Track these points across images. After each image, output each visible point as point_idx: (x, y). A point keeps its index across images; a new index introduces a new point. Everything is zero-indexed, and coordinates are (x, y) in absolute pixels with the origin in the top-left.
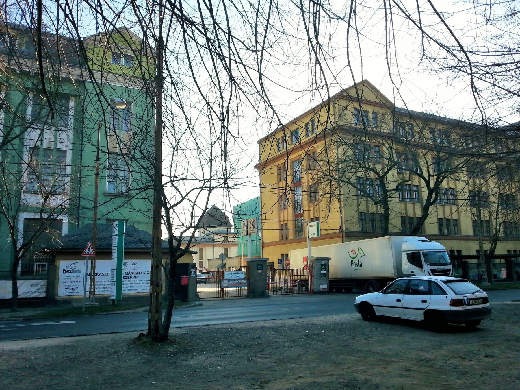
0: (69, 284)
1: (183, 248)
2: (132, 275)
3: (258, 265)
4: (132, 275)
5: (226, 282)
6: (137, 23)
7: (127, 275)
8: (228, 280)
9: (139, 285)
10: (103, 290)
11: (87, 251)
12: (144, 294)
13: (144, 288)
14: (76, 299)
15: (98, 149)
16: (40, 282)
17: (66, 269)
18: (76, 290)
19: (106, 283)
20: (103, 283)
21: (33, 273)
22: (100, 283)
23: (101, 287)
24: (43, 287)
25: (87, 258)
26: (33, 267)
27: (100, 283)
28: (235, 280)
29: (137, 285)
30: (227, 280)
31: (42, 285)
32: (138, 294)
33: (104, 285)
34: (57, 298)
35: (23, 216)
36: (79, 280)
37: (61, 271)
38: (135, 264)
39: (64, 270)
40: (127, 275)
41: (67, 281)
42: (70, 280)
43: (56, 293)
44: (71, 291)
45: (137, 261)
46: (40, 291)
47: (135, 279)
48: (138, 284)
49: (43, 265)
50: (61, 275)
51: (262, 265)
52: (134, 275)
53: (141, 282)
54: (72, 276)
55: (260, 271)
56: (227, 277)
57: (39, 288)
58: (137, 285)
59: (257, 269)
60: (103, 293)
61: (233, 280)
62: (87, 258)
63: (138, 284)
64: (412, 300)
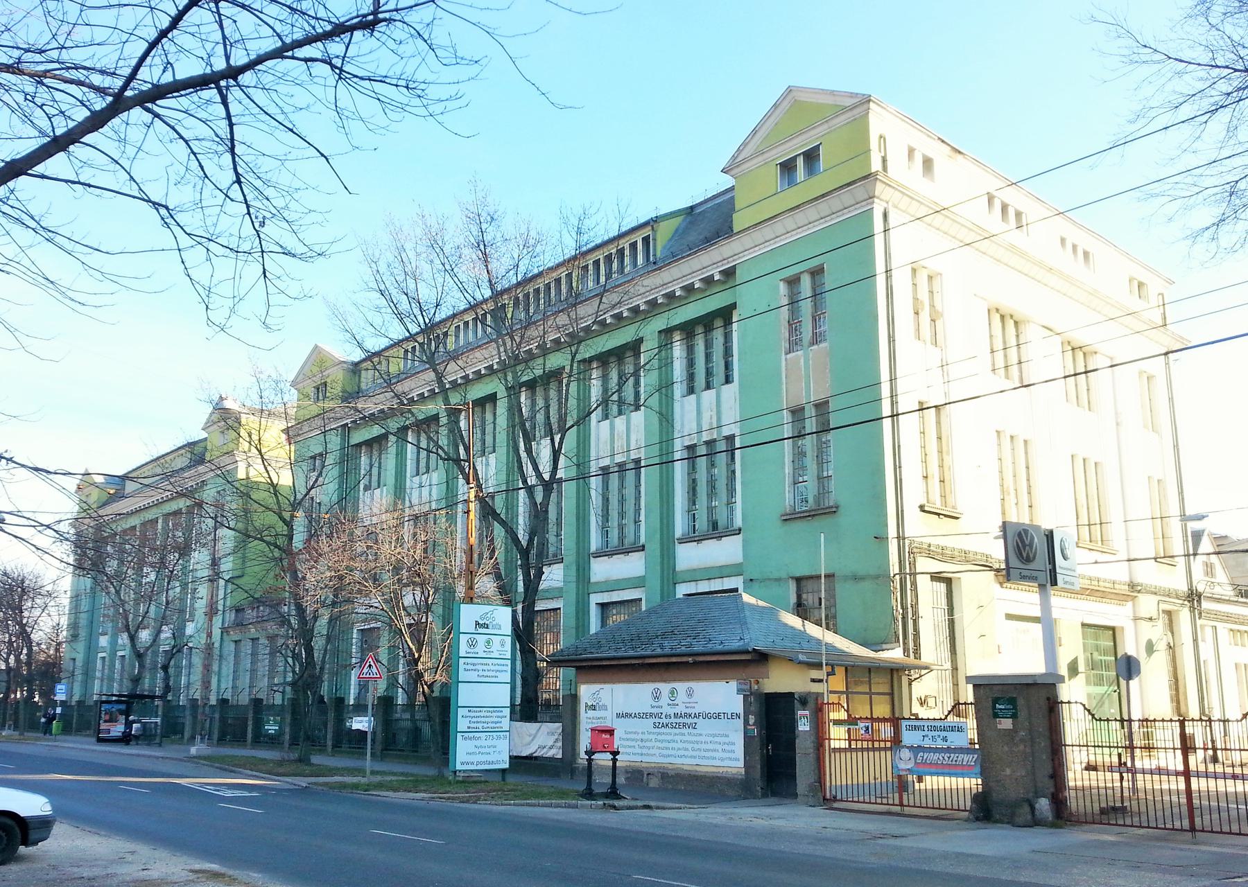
2: (686, 720)
3: (996, 701)
4: (686, 720)
5: (905, 754)
6: (1177, 774)
7: (678, 720)
8: (916, 750)
9: (699, 746)
13: (707, 754)
15: (220, 15)
20: (640, 736)
28: (936, 750)
29: (696, 746)
30: (911, 748)
32: (698, 769)
35: (595, 599)
38: (690, 693)
40: (678, 720)
45: (693, 684)
47: (691, 730)
48: (697, 742)
51: (1012, 701)
52: (689, 721)
53: (703, 739)
55: (1006, 724)
56: (909, 738)
58: (696, 746)
59: (996, 716)
60: (694, 762)
61: (930, 750)
63: (697, 742)
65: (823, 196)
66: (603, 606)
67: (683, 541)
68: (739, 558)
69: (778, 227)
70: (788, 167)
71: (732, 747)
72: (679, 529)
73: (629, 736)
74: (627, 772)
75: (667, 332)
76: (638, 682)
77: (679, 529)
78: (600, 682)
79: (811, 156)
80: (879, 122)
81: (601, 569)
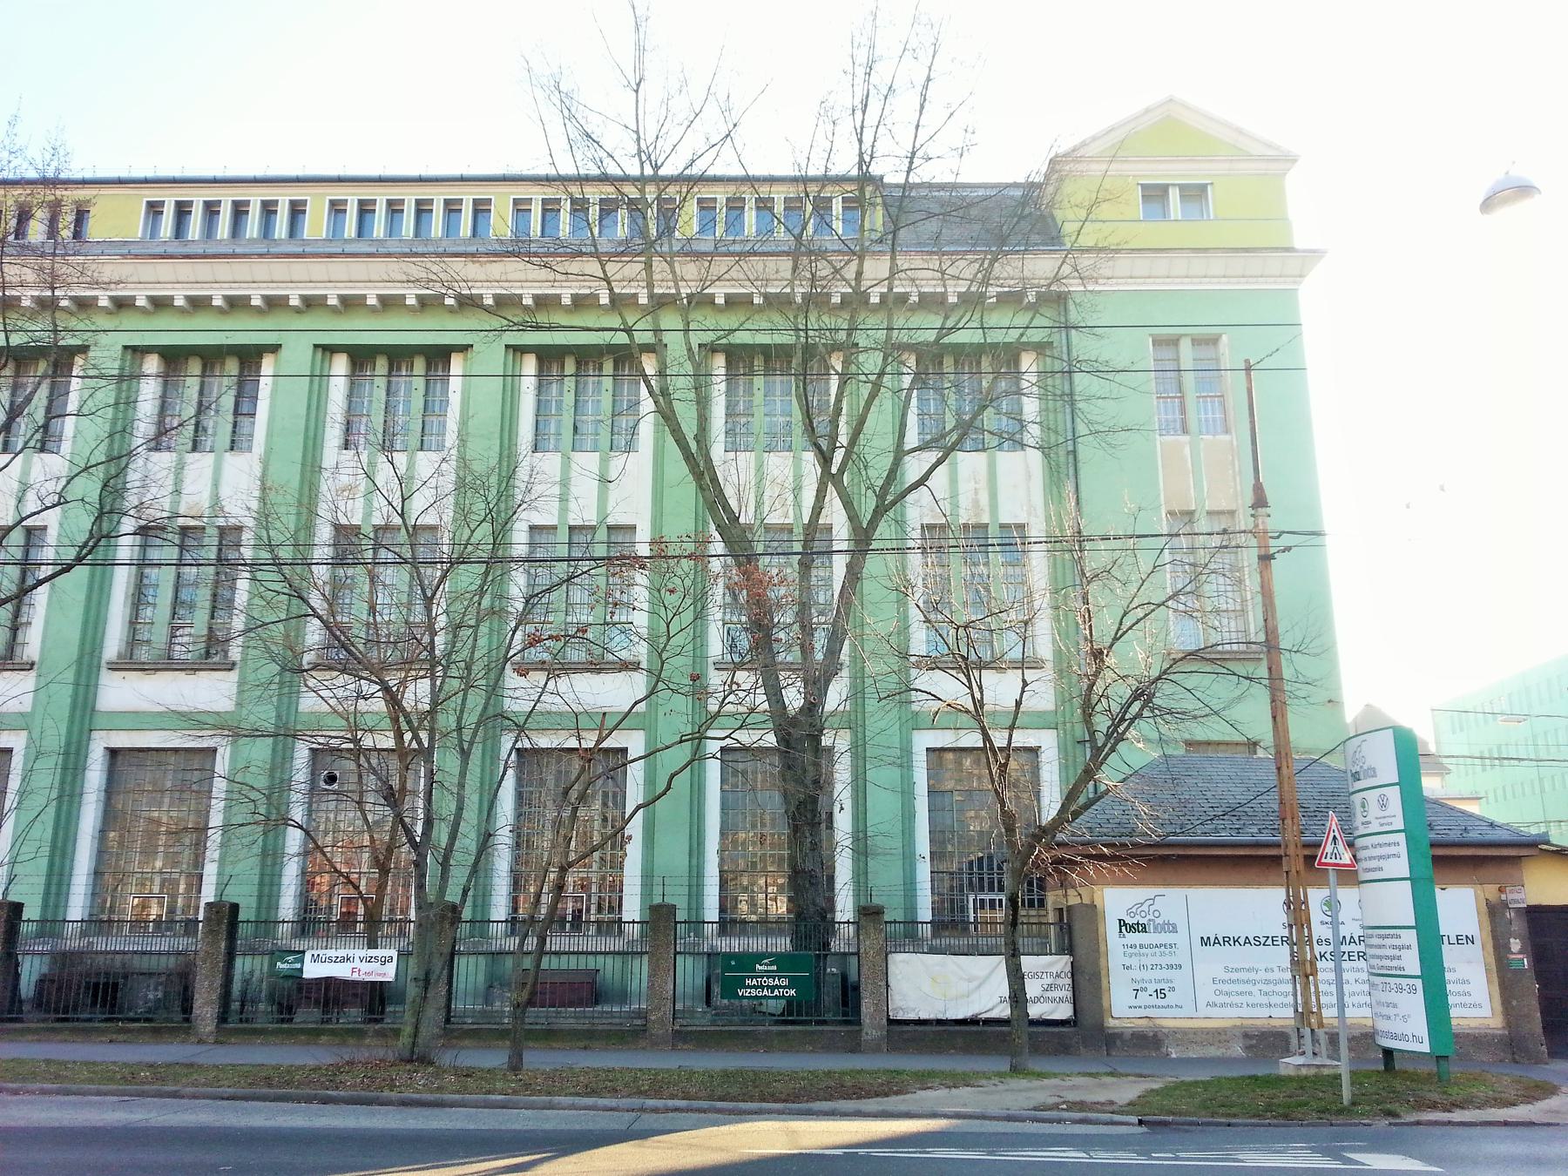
0: (1148, 975)
1: (112, 834)
10: (1265, 1000)
11: (1329, 849)
12: (1473, 1024)
14: (1175, 1031)
16: (1051, 964)
17: (1129, 921)
18: (1171, 998)
19: (1270, 976)
20: (1262, 975)
21: (966, 929)
22: (1252, 976)
23: (1255, 989)
24: (1060, 981)
25: (1332, 877)
26: (964, 909)
27: (1252, 976)
31: (1058, 976)
33: (1267, 982)
34: (1111, 1023)
35: (925, 740)
36: (1173, 960)
37: (1111, 928)
39: (1122, 923)
41: (1134, 962)
42: (1144, 961)
43: (1105, 1004)
44: (1154, 1001)
46: (1049, 994)
49: (992, 902)
50: (1115, 944)
54: (1150, 946)
57: (1050, 987)
60: (1265, 1012)
62: (1332, 877)
64: (544, 899)
65: (1247, 250)
66: (113, 753)
67: (114, 667)
68: (26, 704)
69: (1217, 264)
70: (1155, 194)
71: (1466, 988)
72: (112, 646)
73: (1234, 976)
74: (1246, 1036)
75: (137, 352)
76: (1247, 884)
77: (112, 646)
78: (1155, 884)
79: (1195, 194)
80: (1294, 183)
81: (120, 692)
